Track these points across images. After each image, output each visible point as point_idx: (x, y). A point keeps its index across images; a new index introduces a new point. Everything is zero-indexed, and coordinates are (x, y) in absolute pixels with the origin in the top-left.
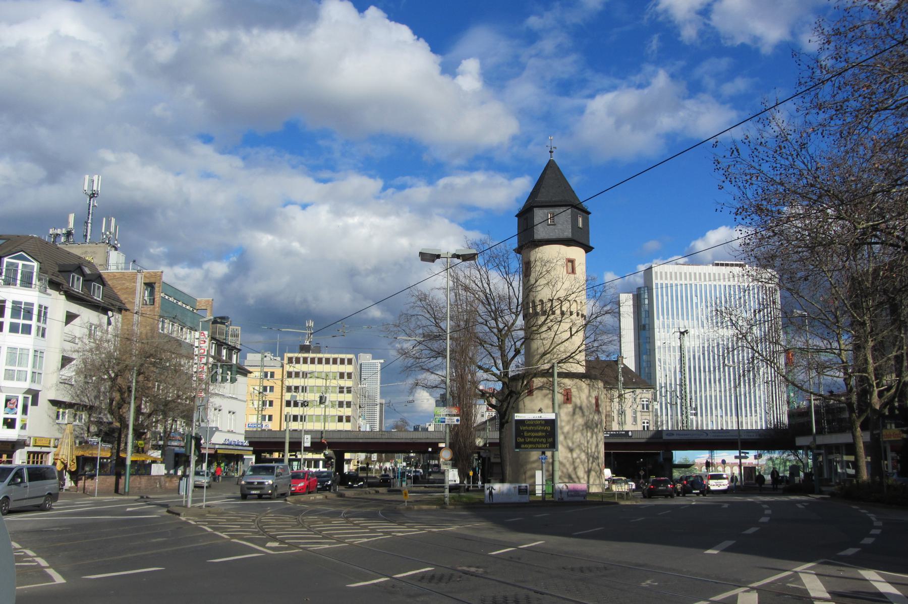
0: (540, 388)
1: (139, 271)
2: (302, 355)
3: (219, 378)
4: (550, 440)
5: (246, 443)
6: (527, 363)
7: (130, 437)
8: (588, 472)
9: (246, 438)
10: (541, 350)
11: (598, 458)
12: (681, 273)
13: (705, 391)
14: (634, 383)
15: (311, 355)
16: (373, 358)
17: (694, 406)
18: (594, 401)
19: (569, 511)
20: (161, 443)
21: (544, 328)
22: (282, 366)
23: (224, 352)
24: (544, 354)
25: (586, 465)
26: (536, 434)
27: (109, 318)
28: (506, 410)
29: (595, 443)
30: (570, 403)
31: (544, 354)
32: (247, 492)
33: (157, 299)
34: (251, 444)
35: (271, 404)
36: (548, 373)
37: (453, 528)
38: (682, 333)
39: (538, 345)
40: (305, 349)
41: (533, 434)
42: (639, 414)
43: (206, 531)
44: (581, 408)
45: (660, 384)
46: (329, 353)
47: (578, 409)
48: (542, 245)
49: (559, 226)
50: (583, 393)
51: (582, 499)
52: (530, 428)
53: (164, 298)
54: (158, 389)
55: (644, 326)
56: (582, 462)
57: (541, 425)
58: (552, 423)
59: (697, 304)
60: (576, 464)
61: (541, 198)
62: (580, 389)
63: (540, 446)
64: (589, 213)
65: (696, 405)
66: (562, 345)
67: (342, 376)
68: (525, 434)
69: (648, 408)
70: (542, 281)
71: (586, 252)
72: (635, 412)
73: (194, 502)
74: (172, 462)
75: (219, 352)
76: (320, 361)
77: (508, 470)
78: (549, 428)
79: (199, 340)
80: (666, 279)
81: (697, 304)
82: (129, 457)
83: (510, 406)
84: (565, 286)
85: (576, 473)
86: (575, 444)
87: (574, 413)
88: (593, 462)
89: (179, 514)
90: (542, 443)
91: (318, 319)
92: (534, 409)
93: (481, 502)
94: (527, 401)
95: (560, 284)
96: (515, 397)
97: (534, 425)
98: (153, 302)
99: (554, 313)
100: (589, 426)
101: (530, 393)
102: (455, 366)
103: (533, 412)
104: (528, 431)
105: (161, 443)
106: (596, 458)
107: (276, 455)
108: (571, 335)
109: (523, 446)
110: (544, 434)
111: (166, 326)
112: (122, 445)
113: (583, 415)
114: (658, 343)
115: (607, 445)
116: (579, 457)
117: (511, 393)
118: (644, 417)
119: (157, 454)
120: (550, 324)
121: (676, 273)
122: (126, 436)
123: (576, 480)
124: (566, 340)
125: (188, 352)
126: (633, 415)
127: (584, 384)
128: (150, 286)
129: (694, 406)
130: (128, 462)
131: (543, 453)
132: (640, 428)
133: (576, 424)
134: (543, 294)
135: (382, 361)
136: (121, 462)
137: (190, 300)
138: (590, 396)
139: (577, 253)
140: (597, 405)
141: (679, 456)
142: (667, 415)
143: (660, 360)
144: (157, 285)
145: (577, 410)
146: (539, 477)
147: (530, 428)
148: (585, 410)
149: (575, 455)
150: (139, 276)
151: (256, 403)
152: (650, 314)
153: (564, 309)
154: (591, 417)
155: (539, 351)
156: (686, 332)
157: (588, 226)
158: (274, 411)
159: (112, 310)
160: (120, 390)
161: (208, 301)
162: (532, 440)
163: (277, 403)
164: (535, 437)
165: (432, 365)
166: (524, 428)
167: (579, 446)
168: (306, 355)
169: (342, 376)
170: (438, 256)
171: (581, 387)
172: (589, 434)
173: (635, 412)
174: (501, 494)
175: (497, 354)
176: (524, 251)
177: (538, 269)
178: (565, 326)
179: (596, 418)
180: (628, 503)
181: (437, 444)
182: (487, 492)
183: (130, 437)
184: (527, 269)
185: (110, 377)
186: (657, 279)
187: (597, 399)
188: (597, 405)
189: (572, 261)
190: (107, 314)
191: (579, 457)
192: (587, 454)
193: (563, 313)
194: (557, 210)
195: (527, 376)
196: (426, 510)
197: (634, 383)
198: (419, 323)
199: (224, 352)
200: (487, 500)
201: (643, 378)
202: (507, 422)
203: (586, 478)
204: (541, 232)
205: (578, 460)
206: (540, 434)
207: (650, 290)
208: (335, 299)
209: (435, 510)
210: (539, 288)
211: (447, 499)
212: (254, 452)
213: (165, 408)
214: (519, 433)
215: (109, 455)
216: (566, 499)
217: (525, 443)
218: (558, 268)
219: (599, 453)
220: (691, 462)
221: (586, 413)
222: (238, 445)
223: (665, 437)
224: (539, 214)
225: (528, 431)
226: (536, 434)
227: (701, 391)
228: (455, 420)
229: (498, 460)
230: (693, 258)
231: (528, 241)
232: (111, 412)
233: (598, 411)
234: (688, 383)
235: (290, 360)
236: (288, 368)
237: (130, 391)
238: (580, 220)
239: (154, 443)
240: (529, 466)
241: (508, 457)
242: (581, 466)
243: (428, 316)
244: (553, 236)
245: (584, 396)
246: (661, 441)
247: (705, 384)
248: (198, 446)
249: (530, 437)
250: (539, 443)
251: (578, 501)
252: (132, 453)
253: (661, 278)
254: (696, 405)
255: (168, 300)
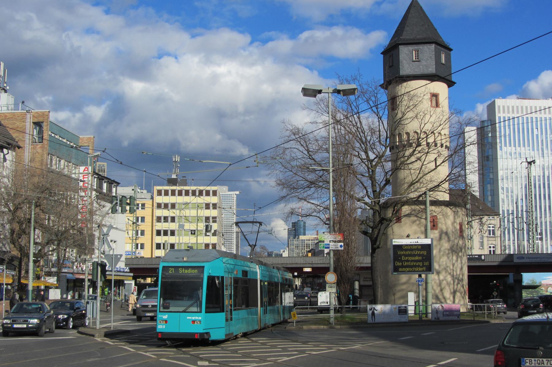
0: (408, 215)
1: (28, 112)
2: (169, 188)
3: (119, 209)
4: (427, 264)
5: (127, 270)
6: (395, 193)
7: (31, 264)
8: (454, 293)
9: (126, 265)
10: (409, 179)
11: (462, 280)
12: (522, 107)
13: (545, 217)
14: (481, 210)
15: (177, 188)
16: (229, 191)
17: (539, 231)
18: (458, 227)
19: (436, 329)
20: (54, 270)
21: (413, 159)
22: (152, 198)
23: (105, 185)
24: (412, 184)
25: (452, 286)
26: (413, 258)
27: (4, 155)
28: (377, 236)
29: (460, 266)
30: (436, 229)
31: (412, 184)
32: (142, 314)
33: (46, 136)
34: (132, 270)
35: (143, 233)
36: (416, 202)
37: (357, 346)
38: (530, 163)
39: (406, 175)
40: (172, 182)
41: (410, 258)
42: (485, 239)
43: (131, 351)
44: (446, 233)
45: (503, 211)
46: (194, 185)
47: (444, 234)
48: (405, 81)
49: (424, 63)
50: (449, 219)
51: (456, 318)
52: (407, 253)
53: (51, 135)
54: (51, 220)
55: (488, 157)
56: (448, 284)
57: (418, 249)
58: (428, 248)
59: (537, 135)
60: (443, 286)
61: (406, 36)
62: (445, 216)
63: (417, 269)
64: (451, 50)
65: (541, 230)
66: (428, 175)
67: (207, 206)
68: (403, 258)
69: (494, 234)
70: (410, 115)
71: (449, 87)
72: (482, 238)
73: (101, 323)
74: (65, 288)
75: (100, 186)
76: (187, 193)
77: (380, 293)
78: (425, 253)
79: (82, 173)
80: (509, 112)
81: (537, 135)
82: (31, 284)
83: (381, 232)
84: (432, 120)
85: (443, 294)
86: (442, 267)
87: (440, 238)
88: (458, 283)
89: (93, 336)
90: (419, 266)
91: (183, 156)
92: (406, 234)
93: (365, 322)
94: (396, 228)
95: (428, 117)
96: (385, 223)
97: (411, 250)
98: (41, 139)
99: (419, 145)
100: (455, 250)
101: (399, 220)
102: (336, 196)
103: (402, 237)
104: (406, 256)
105: (54, 270)
106: (460, 280)
107: (149, 280)
108: (436, 167)
109: (400, 269)
110: (420, 258)
111: (54, 162)
112: (23, 272)
113: (449, 240)
114: (500, 173)
115: (470, 268)
116: (445, 279)
117: (382, 220)
118: (490, 242)
119: (53, 280)
120: (419, 155)
121: (517, 107)
122: (27, 265)
123: (443, 300)
124: (432, 170)
125: (71, 184)
126: (487, 242)
127: (448, 211)
128: (38, 124)
129: (539, 231)
130: (30, 288)
131: (420, 276)
132: (487, 252)
133: (442, 249)
134: (412, 126)
135: (238, 193)
136: (22, 288)
137: (74, 137)
138: (455, 222)
139: (440, 88)
140: (461, 231)
141: (528, 278)
142: (509, 240)
143: (503, 189)
144: (44, 125)
145: (443, 235)
146: (412, 298)
147: (407, 253)
148: (451, 236)
149: (441, 277)
150: (28, 116)
151: (130, 232)
152: (493, 146)
153: (429, 141)
154: (456, 241)
155: (406, 181)
156: (534, 162)
157: (450, 62)
158: (145, 239)
159: (7, 148)
160: (20, 223)
161: (90, 138)
162: (409, 263)
163: (148, 233)
164: (412, 261)
165: (305, 195)
166: (402, 253)
167: (445, 269)
168: (174, 188)
169: (207, 206)
170: (320, 92)
171: (446, 213)
172: (455, 258)
173: (482, 238)
174: (383, 314)
175: (368, 183)
176: (390, 87)
177: (404, 103)
178: (431, 157)
179: (461, 242)
180: (497, 321)
181: (302, 268)
182: (370, 312)
183: (31, 264)
184: (393, 102)
185: (10, 210)
186: (499, 112)
187: (461, 225)
188: (461, 231)
189: (435, 96)
190: (3, 152)
191: (445, 279)
192: (453, 276)
193: (428, 144)
194: (421, 47)
195: (396, 205)
196: (315, 330)
197: (481, 210)
198: (293, 155)
199: (105, 185)
200: (370, 320)
201: (484, 205)
202: (378, 247)
203: (452, 298)
204: (406, 69)
205: (444, 282)
206: (417, 258)
207: (493, 124)
208: (197, 138)
209: (323, 330)
210: (407, 122)
211: (332, 320)
212: (134, 278)
213: (58, 238)
214: (397, 258)
215: (11, 281)
216: (442, 318)
217: (403, 266)
218: (425, 102)
219: (463, 275)
220: (538, 284)
221: (452, 238)
222: (120, 271)
223: (516, 260)
224: (404, 51)
225: (406, 256)
226: (413, 258)
227: (541, 217)
228: (340, 246)
229: (370, 283)
230: (525, 95)
231: (393, 77)
232: (13, 242)
233: (461, 236)
234: (534, 210)
235: (159, 193)
236: (159, 199)
237: (29, 222)
238: (443, 56)
239: (47, 270)
240: (399, 288)
241: (379, 281)
242: (447, 288)
243: (301, 148)
244: (418, 72)
245: (449, 222)
246: (512, 264)
247: (545, 210)
248: (104, 271)
249: (408, 261)
250: (415, 266)
251: (448, 320)
252: (34, 279)
253: (504, 112)
254: (541, 230)
255: (54, 137)
